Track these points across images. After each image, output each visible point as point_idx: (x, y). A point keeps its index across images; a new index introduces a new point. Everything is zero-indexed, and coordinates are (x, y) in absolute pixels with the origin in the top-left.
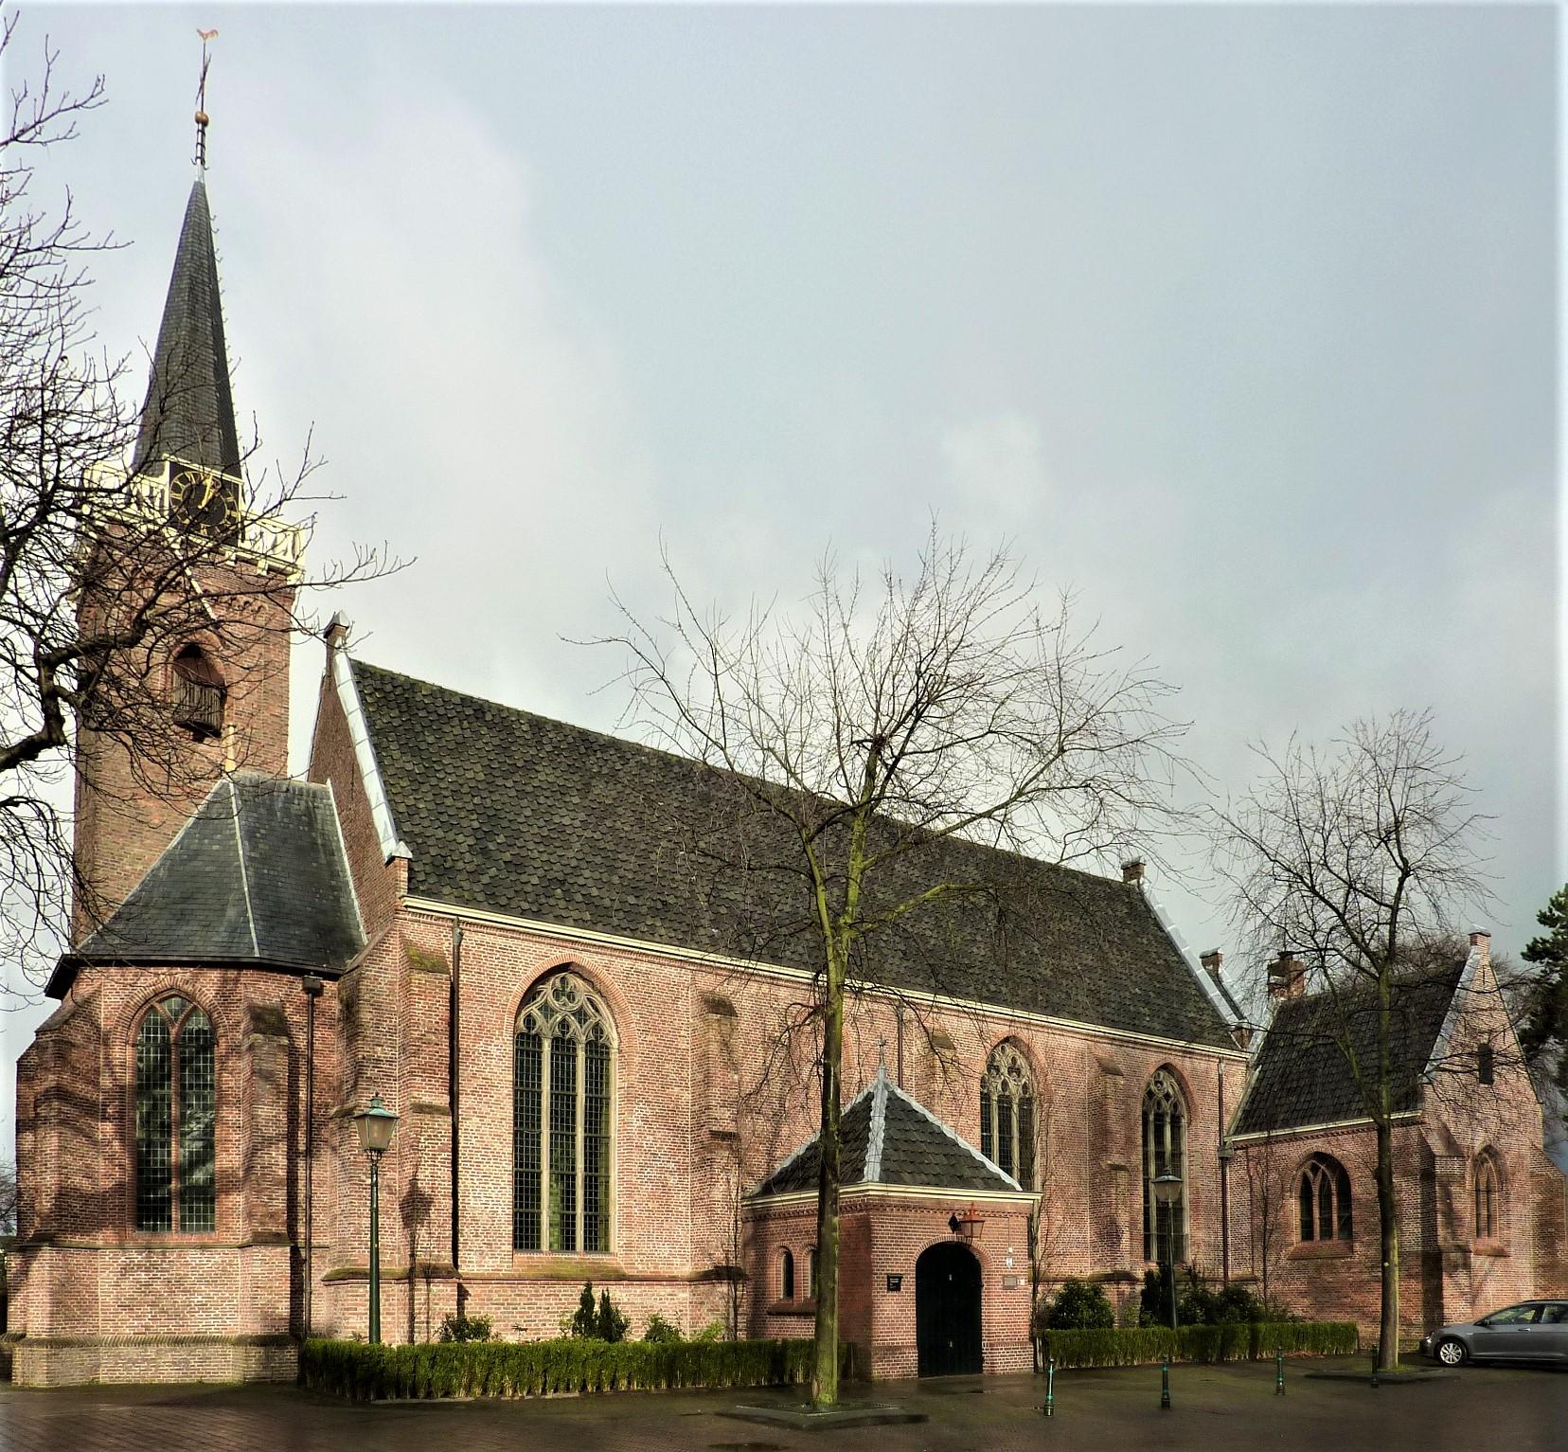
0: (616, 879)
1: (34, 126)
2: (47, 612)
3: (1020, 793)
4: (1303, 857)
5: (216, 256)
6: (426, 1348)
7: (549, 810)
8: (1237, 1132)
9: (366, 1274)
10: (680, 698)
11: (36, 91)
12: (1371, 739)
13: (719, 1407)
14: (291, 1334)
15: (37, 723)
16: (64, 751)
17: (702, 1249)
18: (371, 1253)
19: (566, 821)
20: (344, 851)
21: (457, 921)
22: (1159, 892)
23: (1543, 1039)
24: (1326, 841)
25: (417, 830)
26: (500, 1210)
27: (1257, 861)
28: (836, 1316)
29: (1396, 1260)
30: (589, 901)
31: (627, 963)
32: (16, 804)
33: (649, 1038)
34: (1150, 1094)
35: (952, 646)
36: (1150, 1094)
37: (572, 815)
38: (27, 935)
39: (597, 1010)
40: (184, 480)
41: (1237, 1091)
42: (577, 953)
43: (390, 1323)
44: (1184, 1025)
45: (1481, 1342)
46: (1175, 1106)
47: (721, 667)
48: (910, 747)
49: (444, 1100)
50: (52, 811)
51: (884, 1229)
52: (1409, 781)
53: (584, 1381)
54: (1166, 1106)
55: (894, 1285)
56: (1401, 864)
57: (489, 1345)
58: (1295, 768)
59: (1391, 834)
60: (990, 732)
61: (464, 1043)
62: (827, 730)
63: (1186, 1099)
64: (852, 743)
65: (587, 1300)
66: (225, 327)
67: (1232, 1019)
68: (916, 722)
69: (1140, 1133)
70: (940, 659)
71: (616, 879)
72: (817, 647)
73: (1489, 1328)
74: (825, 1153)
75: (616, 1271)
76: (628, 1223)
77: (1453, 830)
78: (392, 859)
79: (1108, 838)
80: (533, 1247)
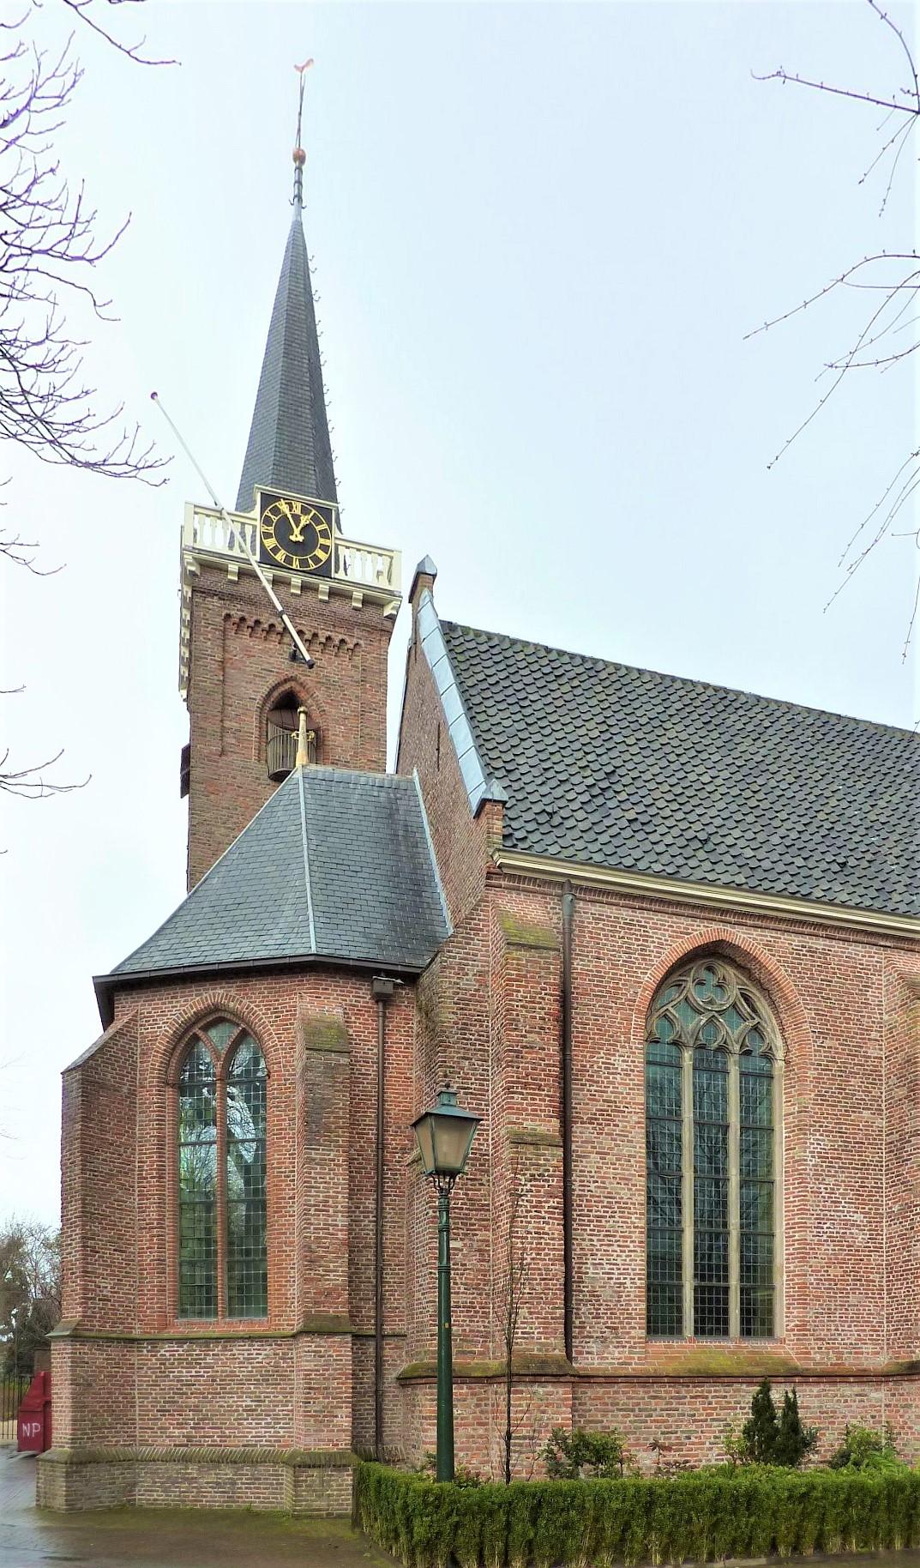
14: (355, 1450)
26: (628, 1282)
31: (796, 941)
33: (827, 1043)
39: (754, 1010)
40: (276, 511)
42: (728, 927)
43: (481, 1437)
61: (579, 1056)
65: (762, 1407)
75: (785, 1363)
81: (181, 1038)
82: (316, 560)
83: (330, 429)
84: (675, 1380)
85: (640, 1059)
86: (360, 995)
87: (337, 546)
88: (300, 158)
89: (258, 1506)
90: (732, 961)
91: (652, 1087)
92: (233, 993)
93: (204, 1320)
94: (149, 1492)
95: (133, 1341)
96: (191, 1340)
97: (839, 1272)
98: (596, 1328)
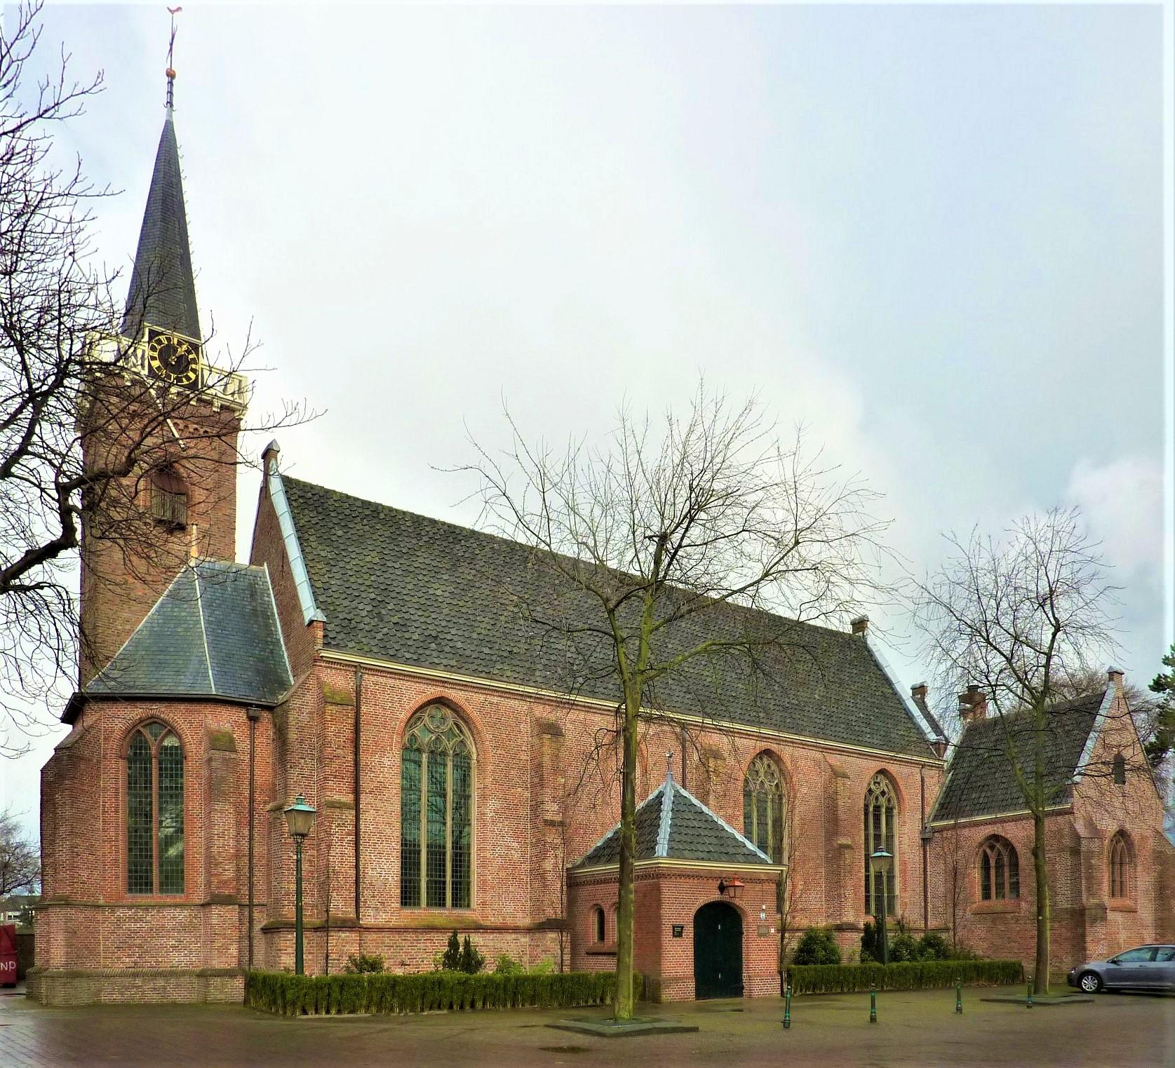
0: (475, 636)
1: (53, 107)
2: (64, 452)
3: (766, 574)
4: (981, 617)
5: (182, 175)
6: (335, 979)
7: (426, 584)
8: (936, 819)
9: (293, 925)
10: (517, 509)
11: (55, 81)
12: (1033, 529)
13: (547, 1021)
15: (58, 531)
16: (77, 550)
17: (537, 907)
18: (297, 909)
19: (439, 592)
20: (276, 616)
21: (357, 668)
22: (874, 641)
23: (1165, 750)
24: (998, 605)
25: (329, 600)
27: (947, 620)
28: (632, 955)
29: (1048, 914)
30: (455, 652)
31: (482, 697)
32: (42, 588)
33: (499, 752)
34: (870, 791)
35: (715, 468)
36: (870, 791)
37: (443, 588)
38: (49, 681)
39: (461, 731)
40: (159, 342)
41: (935, 792)
43: (310, 960)
44: (896, 741)
45: (1113, 975)
46: (889, 800)
47: (548, 486)
48: (686, 542)
49: (349, 798)
50: (67, 592)
51: (669, 891)
52: (1060, 561)
53: (463, 1002)
54: (883, 801)
55: (678, 932)
56: (1054, 622)
57: (381, 977)
58: (976, 551)
59: (1046, 600)
60: (744, 530)
61: (364, 759)
62: (625, 529)
63: (897, 795)
64: (645, 538)
65: (453, 944)
66: (186, 186)
67: (932, 737)
68: (690, 523)
69: (863, 821)
70: (707, 476)
71: (475, 636)
72: (619, 469)
73: (1118, 965)
74: (624, 837)
75: (475, 922)
76: (483, 886)
77: (1092, 597)
78: (311, 622)
79: (832, 607)
80: (414, 904)
81: (129, 732)
82: (188, 378)
83: (194, 275)
84: (415, 930)
85: (398, 760)
86: (241, 715)
87: (202, 369)
88: (171, 75)
89: (179, 1000)
90: (448, 707)
91: (405, 776)
92: (163, 709)
93: (144, 895)
94: (111, 995)
95: (99, 906)
96: (138, 907)
97: (504, 874)
98: (372, 903)
